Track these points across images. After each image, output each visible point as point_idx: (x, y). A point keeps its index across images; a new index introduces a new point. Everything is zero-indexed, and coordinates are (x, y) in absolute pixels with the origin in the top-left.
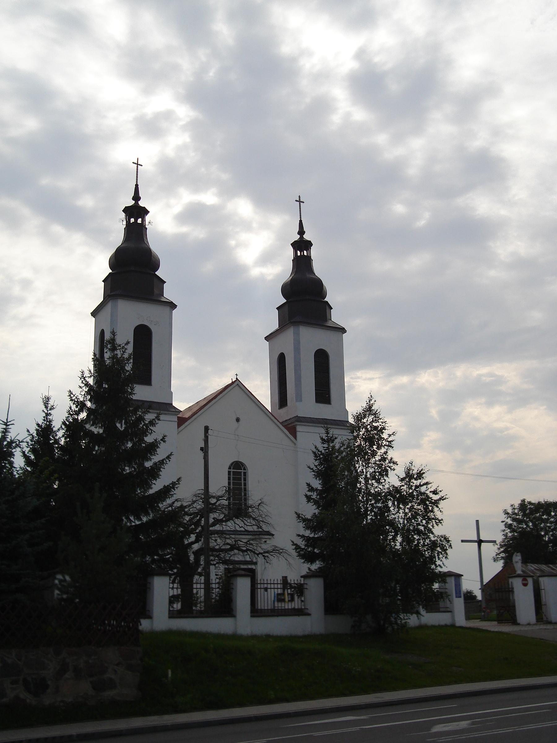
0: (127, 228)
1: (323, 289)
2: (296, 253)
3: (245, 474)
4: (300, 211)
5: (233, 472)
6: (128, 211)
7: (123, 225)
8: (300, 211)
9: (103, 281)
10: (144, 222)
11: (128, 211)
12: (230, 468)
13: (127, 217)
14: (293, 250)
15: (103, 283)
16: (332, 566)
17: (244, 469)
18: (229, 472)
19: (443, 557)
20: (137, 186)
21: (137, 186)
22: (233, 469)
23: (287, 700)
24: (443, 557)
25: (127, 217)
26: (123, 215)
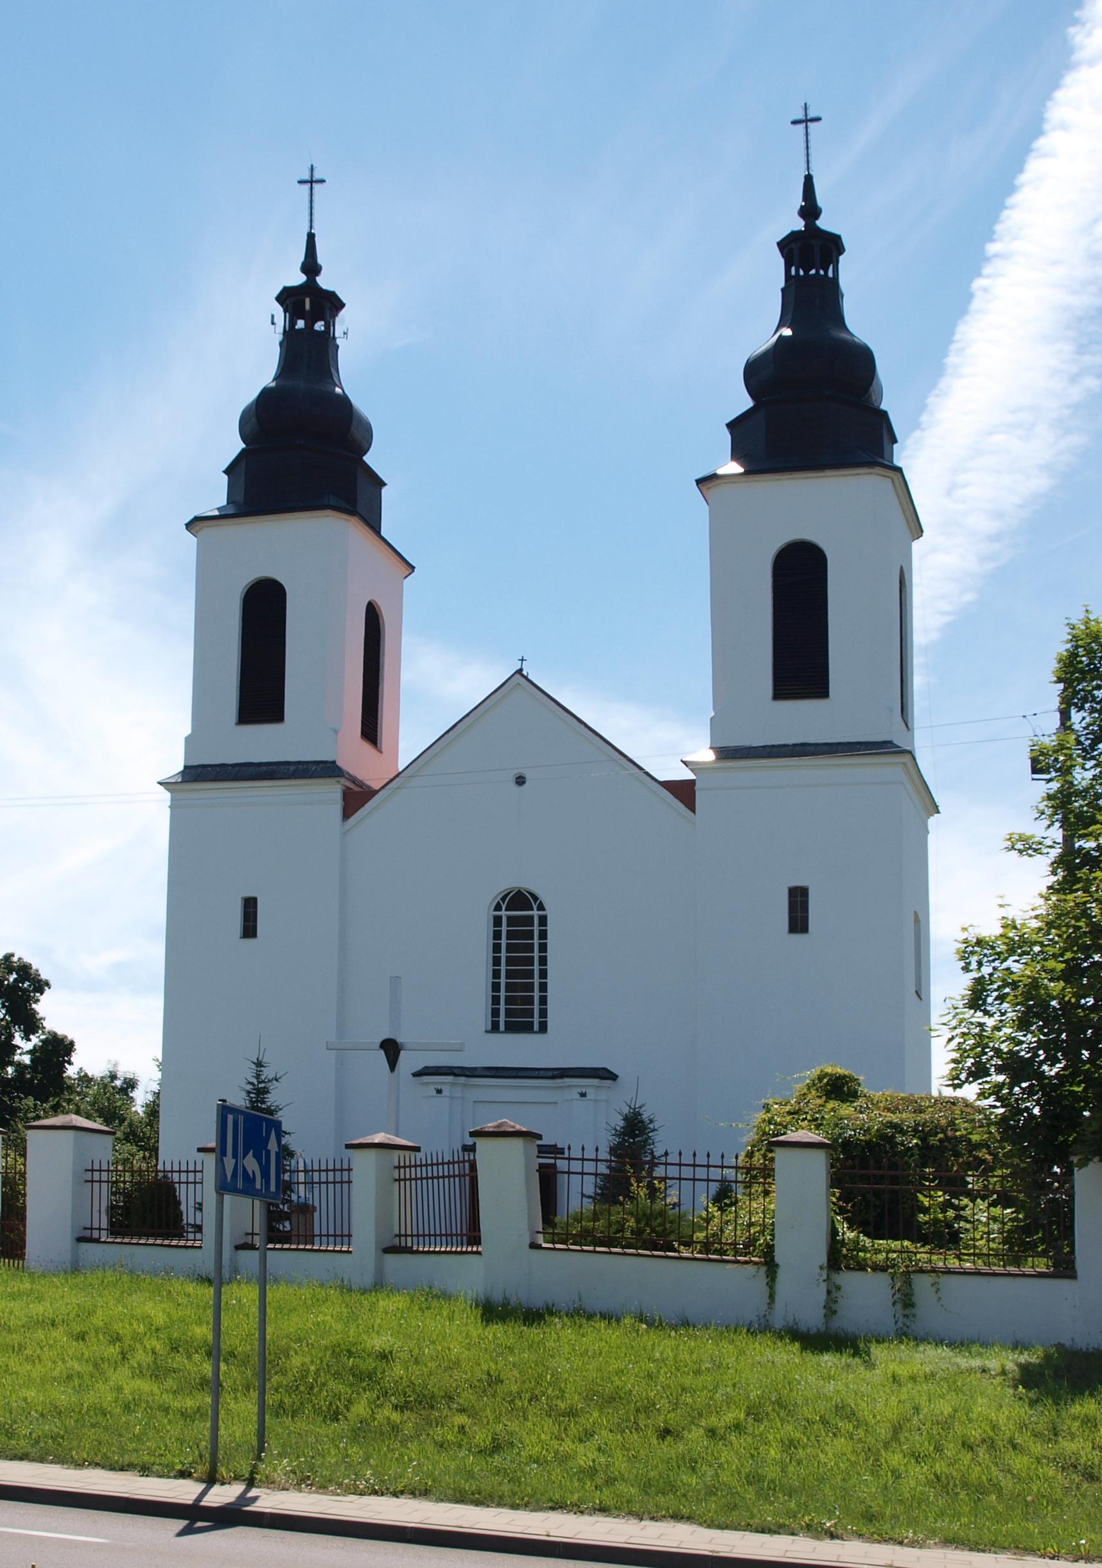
0: (285, 342)
1: (352, 417)
2: (327, 326)
3: (543, 920)
4: (311, 201)
5: (509, 918)
6: (288, 298)
7: (274, 336)
8: (311, 201)
9: (224, 472)
10: (332, 328)
11: (288, 298)
12: (498, 908)
13: (287, 314)
14: (283, 314)
15: (226, 477)
16: (238, 1277)
17: (541, 907)
18: (497, 921)
19: (90, 1363)
20: (311, 237)
21: (311, 237)
22: (506, 910)
23: (577, 1509)
24: (90, 1363)
25: (287, 314)
26: (279, 311)
